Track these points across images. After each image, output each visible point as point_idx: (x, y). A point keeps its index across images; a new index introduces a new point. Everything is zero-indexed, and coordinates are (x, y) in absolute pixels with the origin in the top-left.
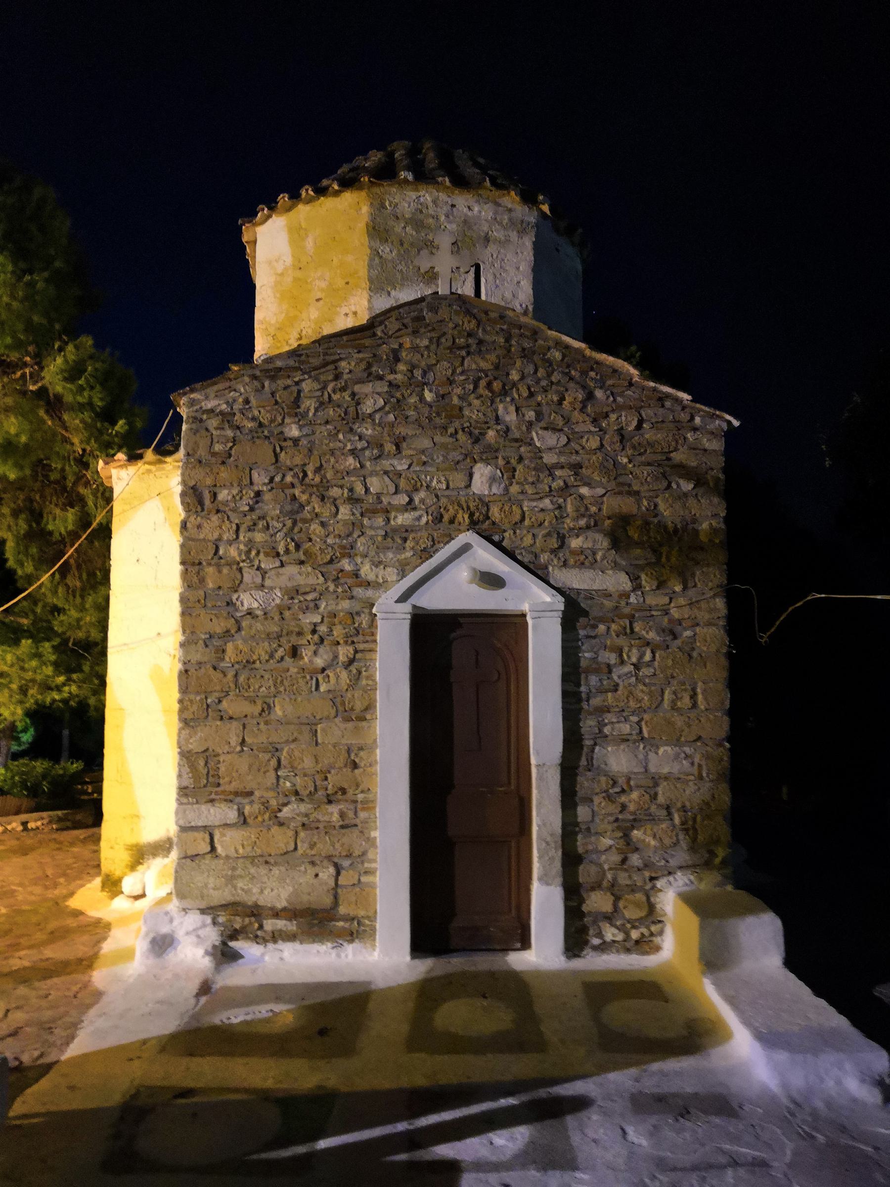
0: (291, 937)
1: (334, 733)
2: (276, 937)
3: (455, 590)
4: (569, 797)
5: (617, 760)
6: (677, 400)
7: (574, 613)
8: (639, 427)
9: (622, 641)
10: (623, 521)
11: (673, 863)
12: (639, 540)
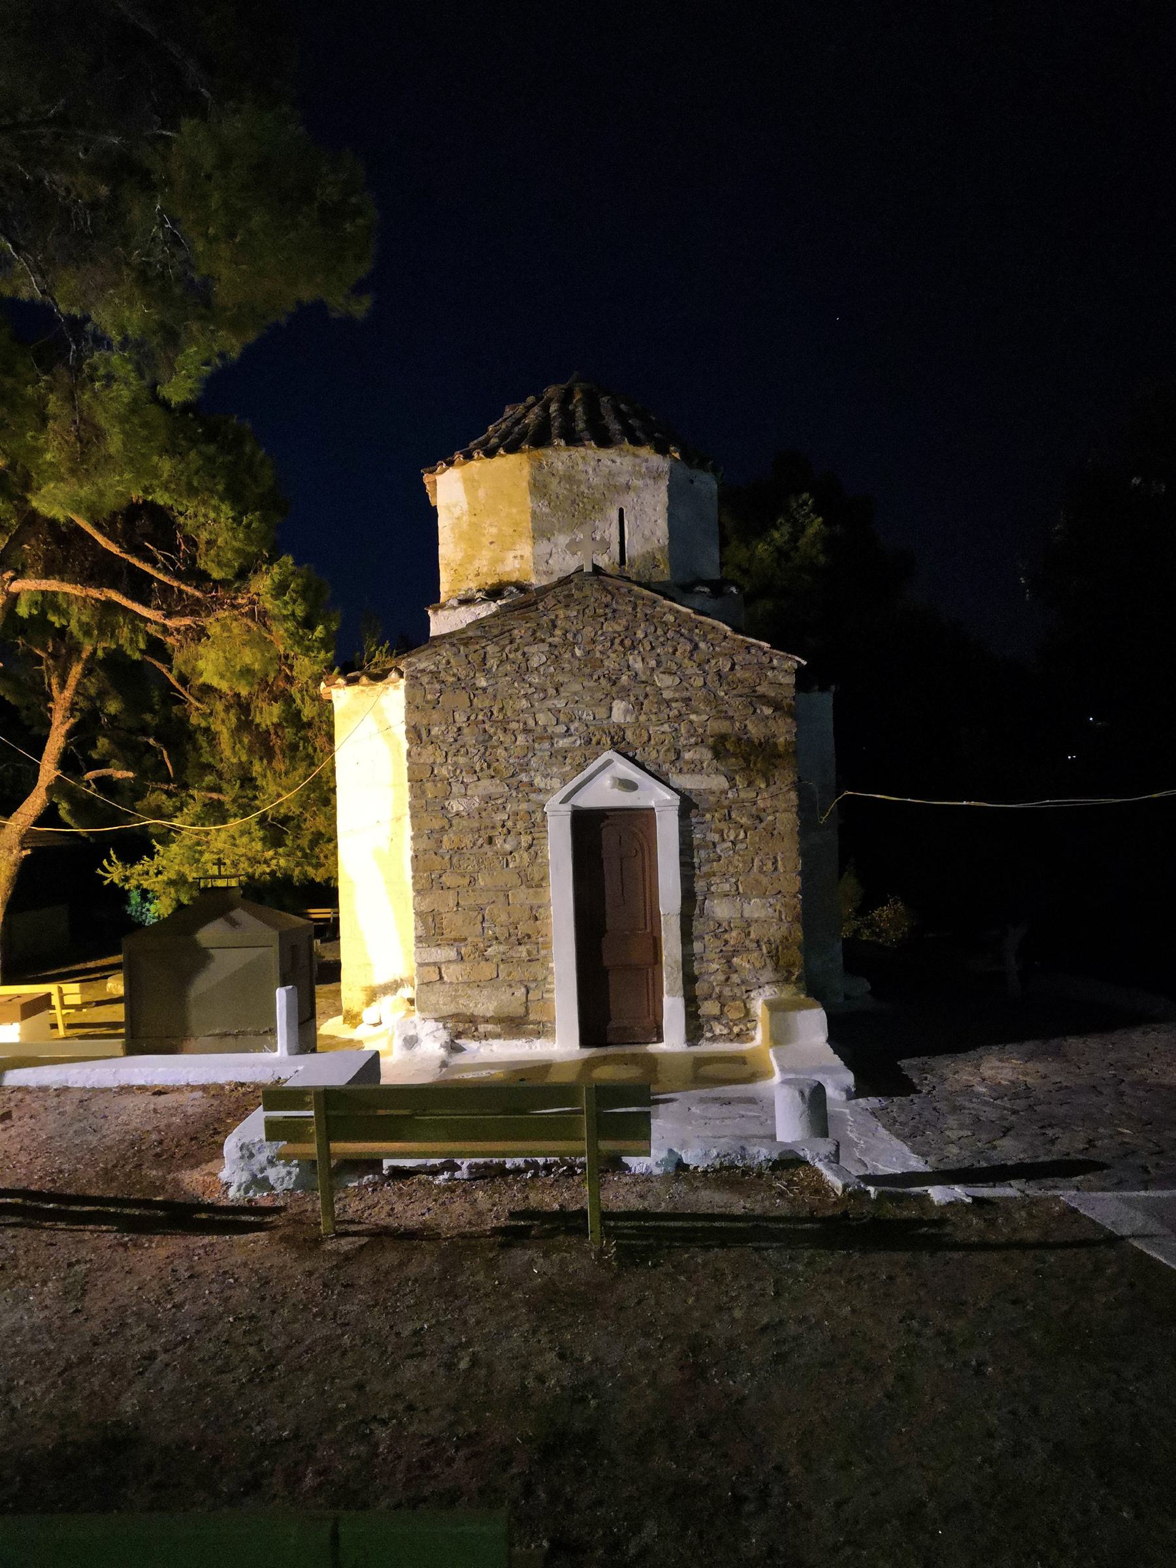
0: (498, 1036)
1: (521, 896)
2: (486, 1036)
3: (602, 793)
4: (687, 936)
5: (721, 909)
6: (760, 648)
7: (688, 806)
8: (732, 668)
9: (723, 826)
10: (722, 738)
11: (763, 980)
12: (742, 754)
